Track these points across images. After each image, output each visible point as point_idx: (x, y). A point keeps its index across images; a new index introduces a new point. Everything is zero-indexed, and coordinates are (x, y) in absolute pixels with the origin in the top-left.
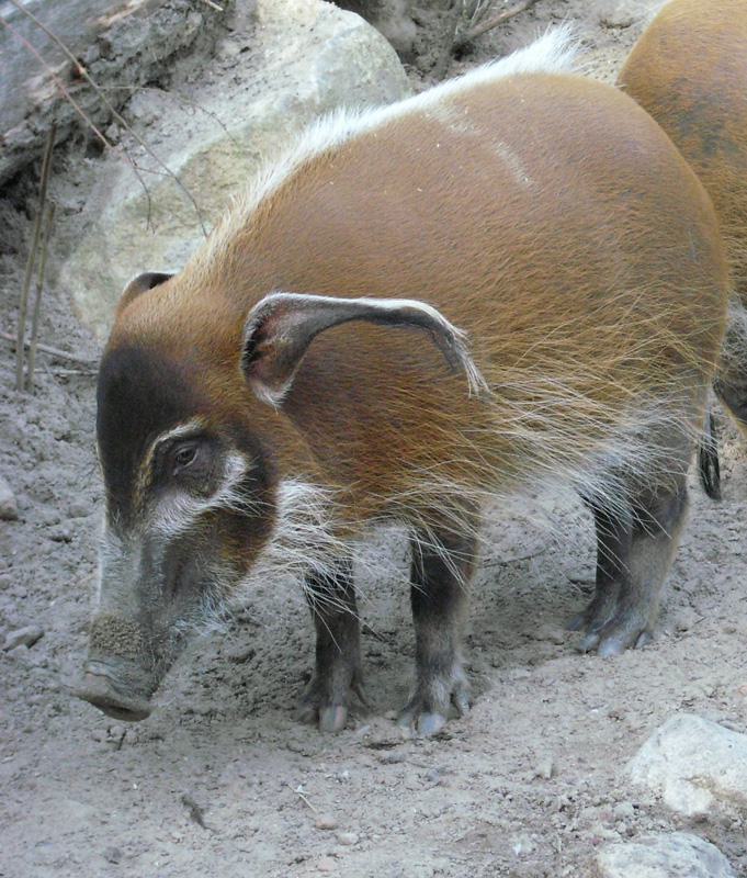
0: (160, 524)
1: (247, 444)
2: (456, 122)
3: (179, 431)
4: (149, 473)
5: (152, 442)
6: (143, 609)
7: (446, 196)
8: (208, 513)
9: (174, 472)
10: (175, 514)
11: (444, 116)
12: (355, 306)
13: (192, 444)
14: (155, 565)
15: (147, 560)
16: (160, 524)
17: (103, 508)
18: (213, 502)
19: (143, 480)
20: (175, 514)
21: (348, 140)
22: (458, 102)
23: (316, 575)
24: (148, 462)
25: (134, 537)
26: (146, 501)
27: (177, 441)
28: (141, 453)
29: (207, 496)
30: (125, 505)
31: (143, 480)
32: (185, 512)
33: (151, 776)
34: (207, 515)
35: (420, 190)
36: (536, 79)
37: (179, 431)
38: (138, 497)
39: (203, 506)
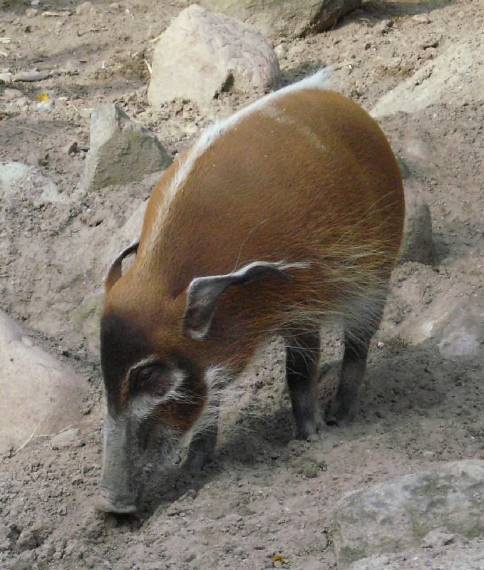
0: (135, 412)
1: (182, 366)
2: (280, 116)
3: (142, 362)
4: (128, 385)
5: (128, 369)
6: (128, 458)
7: (282, 158)
8: (147, 515)
9: (142, 385)
10: (142, 408)
11: (273, 113)
12: (229, 279)
13: (150, 369)
14: (133, 434)
15: (128, 432)
16: (135, 412)
17: (104, 399)
18: (165, 399)
19: (124, 390)
20: (142, 408)
21: (221, 135)
22: (278, 104)
23: (334, 307)
24: (127, 379)
25: (121, 419)
26: (127, 399)
27: (141, 368)
28: (123, 373)
29: (162, 395)
30: (117, 404)
31: (124, 390)
32: (148, 404)
33: (477, 304)
34: (161, 405)
35: (266, 156)
36: (315, 92)
37: (142, 362)
38: (123, 399)
39: (157, 401)
